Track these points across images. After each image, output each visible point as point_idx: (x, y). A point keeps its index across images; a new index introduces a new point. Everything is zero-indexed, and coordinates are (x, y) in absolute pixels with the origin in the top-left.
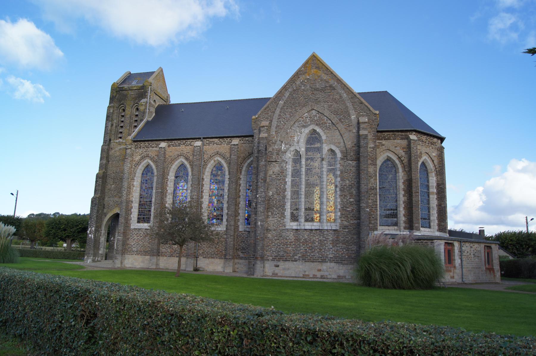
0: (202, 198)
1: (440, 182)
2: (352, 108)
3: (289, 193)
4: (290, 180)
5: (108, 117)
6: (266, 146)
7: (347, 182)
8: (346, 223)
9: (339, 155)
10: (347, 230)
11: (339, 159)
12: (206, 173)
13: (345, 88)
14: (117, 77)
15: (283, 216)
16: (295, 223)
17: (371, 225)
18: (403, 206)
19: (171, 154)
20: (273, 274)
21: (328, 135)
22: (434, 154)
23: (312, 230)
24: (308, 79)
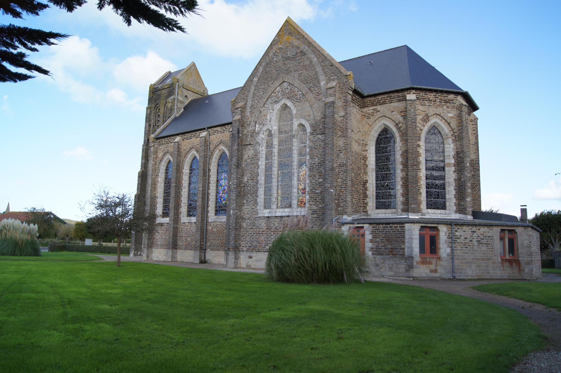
0: (209, 189)
1: (459, 150)
2: (322, 73)
3: (263, 178)
4: (264, 163)
5: (146, 118)
6: (238, 129)
7: (317, 160)
8: (314, 207)
9: (309, 130)
10: (315, 216)
11: (308, 134)
12: (213, 164)
13: (316, 51)
14: (154, 78)
15: (256, 203)
16: (268, 211)
17: (339, 209)
18: (401, 183)
19: (185, 148)
20: (247, 266)
21: (299, 108)
22: (450, 115)
23: (282, 217)
24: (280, 48)
